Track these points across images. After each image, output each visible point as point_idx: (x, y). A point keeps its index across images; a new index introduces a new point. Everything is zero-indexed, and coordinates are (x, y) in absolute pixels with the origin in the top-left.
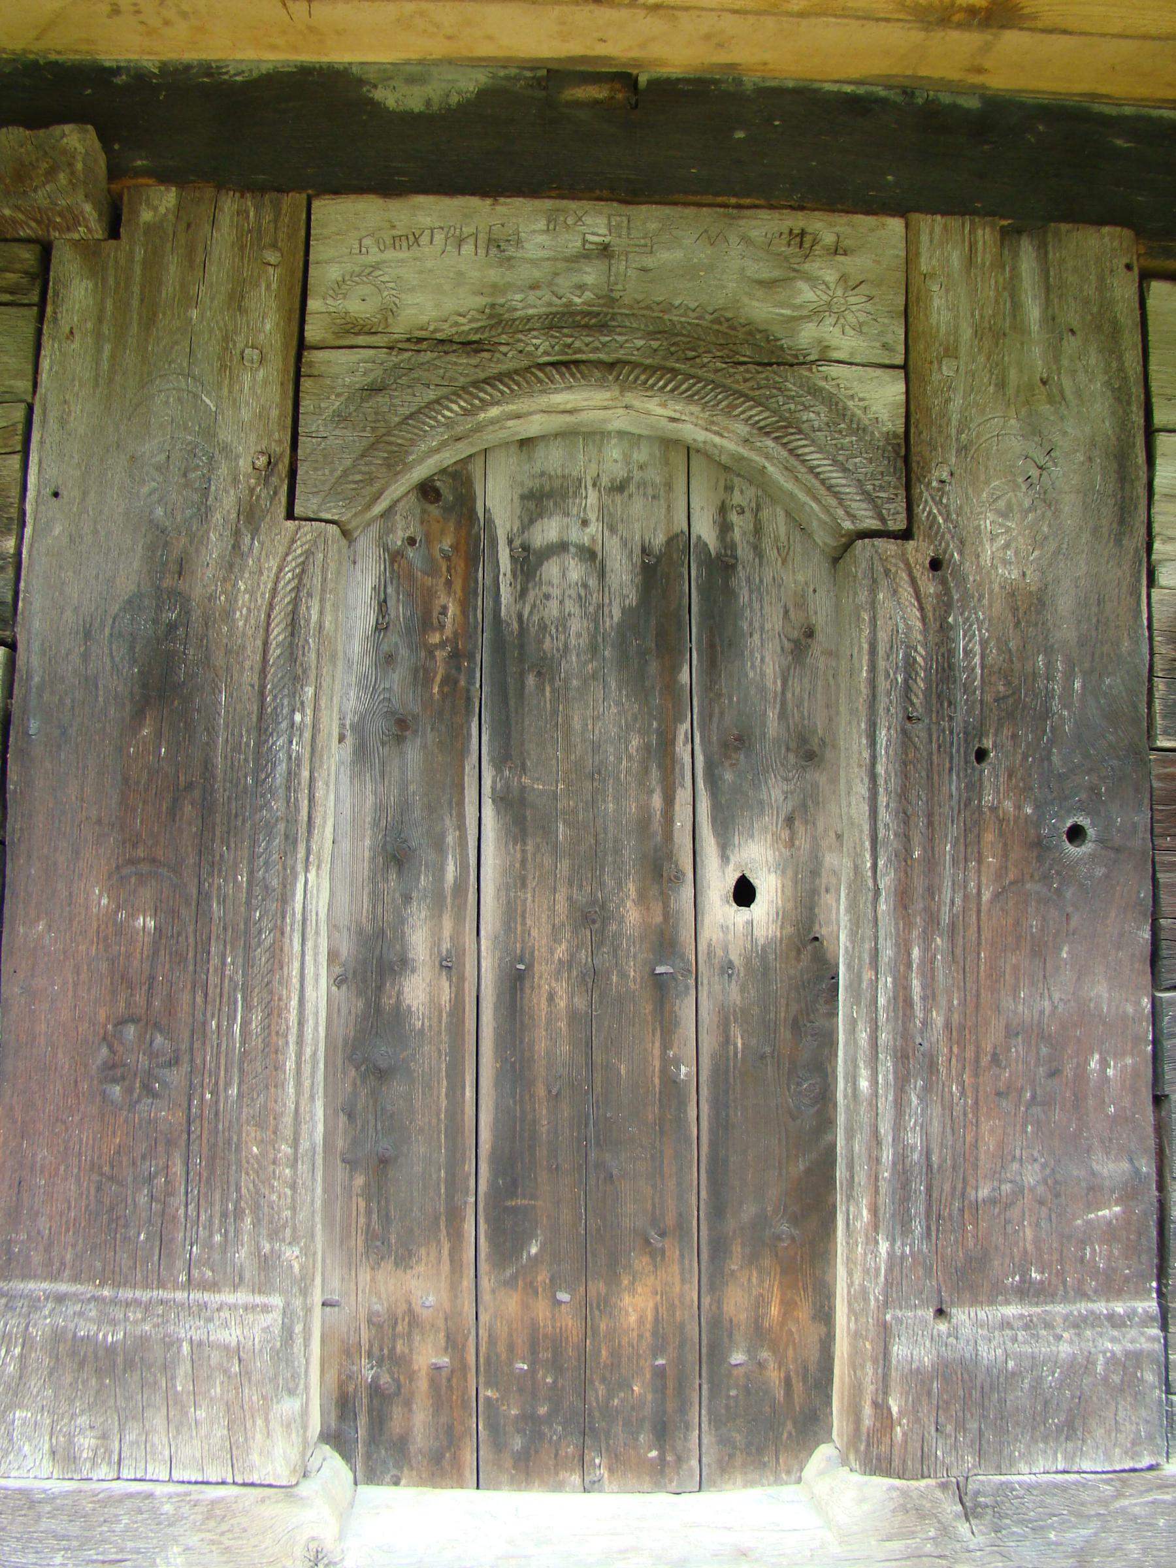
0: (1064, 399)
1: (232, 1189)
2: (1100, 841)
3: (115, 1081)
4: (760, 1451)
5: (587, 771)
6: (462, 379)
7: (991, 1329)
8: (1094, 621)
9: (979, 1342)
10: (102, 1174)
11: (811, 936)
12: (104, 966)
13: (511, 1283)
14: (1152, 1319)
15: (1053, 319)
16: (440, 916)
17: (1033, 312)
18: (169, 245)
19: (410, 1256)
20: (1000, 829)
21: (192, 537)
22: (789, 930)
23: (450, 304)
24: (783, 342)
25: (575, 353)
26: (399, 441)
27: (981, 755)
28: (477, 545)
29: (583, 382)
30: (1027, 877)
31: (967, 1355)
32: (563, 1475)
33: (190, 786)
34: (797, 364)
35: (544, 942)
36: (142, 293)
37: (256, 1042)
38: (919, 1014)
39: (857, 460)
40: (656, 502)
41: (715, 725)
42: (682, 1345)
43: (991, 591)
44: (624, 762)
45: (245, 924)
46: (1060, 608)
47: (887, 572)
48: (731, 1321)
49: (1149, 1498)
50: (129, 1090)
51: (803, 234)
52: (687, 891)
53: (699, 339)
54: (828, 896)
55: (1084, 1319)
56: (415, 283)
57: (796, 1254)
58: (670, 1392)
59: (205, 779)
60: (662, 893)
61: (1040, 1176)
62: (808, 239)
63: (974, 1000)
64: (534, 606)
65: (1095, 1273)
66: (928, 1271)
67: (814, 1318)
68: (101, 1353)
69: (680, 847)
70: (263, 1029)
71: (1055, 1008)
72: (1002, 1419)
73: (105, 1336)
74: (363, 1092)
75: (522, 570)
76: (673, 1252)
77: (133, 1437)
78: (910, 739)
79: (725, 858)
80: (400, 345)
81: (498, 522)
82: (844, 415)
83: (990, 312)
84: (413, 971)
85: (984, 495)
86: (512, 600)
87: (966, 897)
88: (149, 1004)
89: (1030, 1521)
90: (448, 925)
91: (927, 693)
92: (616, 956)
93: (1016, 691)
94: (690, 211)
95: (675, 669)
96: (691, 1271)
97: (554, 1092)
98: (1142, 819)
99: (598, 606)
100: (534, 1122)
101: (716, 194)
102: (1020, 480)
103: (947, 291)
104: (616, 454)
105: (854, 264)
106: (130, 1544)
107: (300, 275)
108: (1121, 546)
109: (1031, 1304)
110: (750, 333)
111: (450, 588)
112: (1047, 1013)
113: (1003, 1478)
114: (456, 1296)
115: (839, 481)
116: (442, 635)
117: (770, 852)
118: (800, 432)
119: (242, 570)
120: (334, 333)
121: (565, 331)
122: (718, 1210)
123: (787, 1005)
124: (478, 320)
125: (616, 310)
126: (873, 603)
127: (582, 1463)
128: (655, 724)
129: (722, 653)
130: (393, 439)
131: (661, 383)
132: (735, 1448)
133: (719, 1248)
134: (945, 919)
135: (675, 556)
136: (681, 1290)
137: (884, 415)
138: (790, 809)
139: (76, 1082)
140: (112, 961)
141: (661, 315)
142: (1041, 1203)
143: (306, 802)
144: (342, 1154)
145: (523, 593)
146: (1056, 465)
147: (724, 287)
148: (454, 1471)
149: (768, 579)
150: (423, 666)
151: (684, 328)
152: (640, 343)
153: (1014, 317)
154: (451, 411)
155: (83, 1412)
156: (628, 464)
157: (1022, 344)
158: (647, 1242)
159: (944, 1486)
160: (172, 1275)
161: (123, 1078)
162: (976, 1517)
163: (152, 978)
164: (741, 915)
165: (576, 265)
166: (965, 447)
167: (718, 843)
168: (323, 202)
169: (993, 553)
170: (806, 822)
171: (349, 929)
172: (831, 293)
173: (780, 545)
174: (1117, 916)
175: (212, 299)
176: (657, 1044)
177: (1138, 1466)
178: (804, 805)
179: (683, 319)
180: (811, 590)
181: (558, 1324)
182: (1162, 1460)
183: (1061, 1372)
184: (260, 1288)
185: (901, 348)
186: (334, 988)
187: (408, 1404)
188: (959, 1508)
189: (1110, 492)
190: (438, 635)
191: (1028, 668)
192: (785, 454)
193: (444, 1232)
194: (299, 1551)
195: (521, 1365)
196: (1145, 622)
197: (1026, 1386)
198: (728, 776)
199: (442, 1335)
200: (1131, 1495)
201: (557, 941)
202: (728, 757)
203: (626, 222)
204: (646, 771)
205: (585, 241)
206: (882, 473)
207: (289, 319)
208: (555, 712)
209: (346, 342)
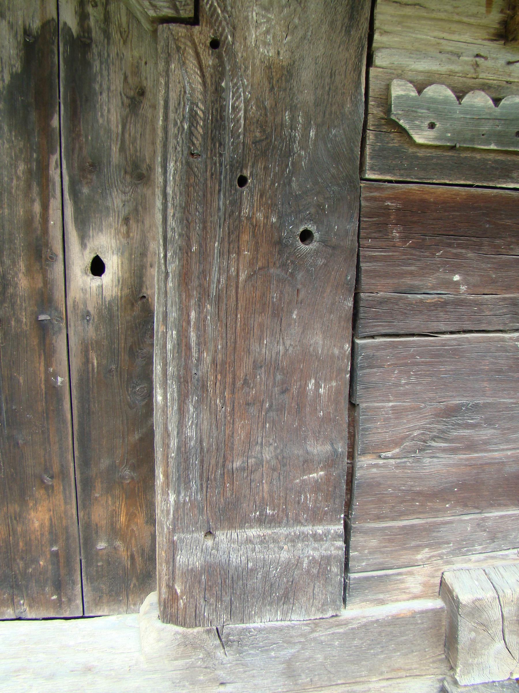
2: (323, 242)
4: (118, 594)
8: (327, 88)
9: (231, 552)
11: (141, 295)
14: (339, 536)
20: (254, 232)
22: (126, 291)
27: (242, 181)
30: (271, 265)
38: (195, 355)
41: (76, 156)
42: (67, 539)
43: (254, 65)
44: (15, 181)
46: (303, 79)
47: (178, 48)
48: (97, 525)
49: (331, 631)
52: (59, 267)
54: (152, 270)
55: (298, 537)
57: (135, 487)
58: (62, 564)
60: (41, 268)
61: (273, 454)
63: (233, 345)
65: (306, 509)
66: (201, 511)
67: (147, 522)
72: (244, 594)
76: (59, 487)
78: (191, 169)
79: (83, 245)
87: (228, 278)
89: (260, 647)
91: (204, 137)
92: (13, 309)
93: (268, 137)
95: (48, 117)
98: (352, 227)
108: (349, 35)
109: (265, 527)
112: (281, 354)
117: (113, 241)
123: (126, 339)
126: (167, 72)
128: (35, 155)
132: (102, 593)
134: (213, 292)
136: (65, 509)
138: (127, 212)
142: (274, 470)
149: (113, 55)
158: (43, 482)
159: (209, 632)
164: (94, 282)
167: (79, 235)
170: (138, 221)
173: (122, 30)
174: (331, 291)
176: (42, 364)
178: (136, 210)
180: (143, 63)
188: (218, 642)
191: (278, 120)
196: (363, 91)
197: (260, 576)
198: (85, 190)
202: (84, 177)
204: (29, 187)
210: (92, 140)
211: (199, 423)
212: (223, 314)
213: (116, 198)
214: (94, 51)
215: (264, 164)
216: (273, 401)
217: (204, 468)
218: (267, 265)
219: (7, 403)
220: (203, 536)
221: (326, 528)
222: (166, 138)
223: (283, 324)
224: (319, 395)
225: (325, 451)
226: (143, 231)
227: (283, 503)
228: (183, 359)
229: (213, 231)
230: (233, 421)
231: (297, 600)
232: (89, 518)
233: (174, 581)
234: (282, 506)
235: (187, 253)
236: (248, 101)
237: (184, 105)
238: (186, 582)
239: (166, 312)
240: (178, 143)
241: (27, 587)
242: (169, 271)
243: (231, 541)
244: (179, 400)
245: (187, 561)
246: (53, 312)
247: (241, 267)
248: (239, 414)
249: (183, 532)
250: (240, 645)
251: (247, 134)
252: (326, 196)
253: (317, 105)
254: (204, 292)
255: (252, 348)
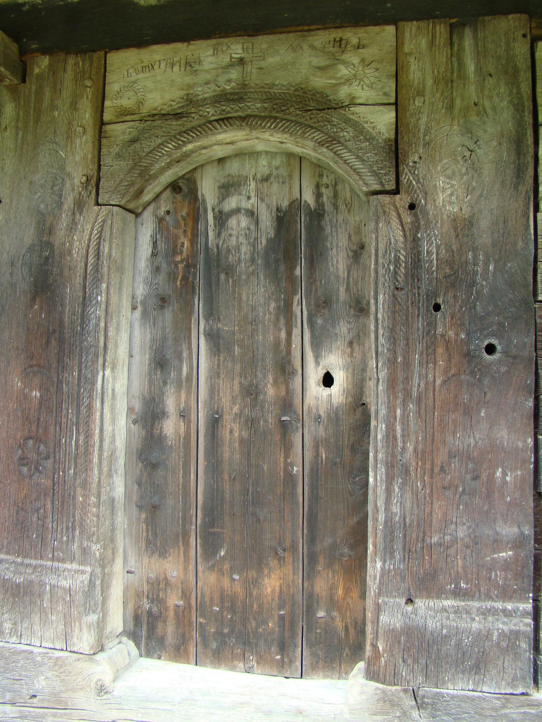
0: (485, 112)
1: (71, 516)
2: (505, 352)
3: (24, 465)
4: (332, 661)
5: (249, 320)
6: (173, 132)
7: (436, 612)
8: (502, 232)
9: (428, 618)
10: (19, 507)
11: (362, 402)
12: (19, 414)
13: (211, 568)
14: (528, 614)
15: (481, 69)
16: (180, 391)
17: (471, 67)
18: (46, 83)
19: (166, 553)
20: (447, 347)
21: (54, 216)
22: (350, 399)
23: (168, 96)
24: (331, 97)
25: (227, 113)
26: (145, 165)
27: (437, 308)
28: (198, 213)
29: (232, 128)
30: (462, 372)
31: (420, 624)
32: (236, 662)
33: (54, 331)
34: (340, 108)
35: (228, 404)
36: (35, 106)
37: (81, 450)
38: (400, 444)
39: (369, 155)
40: (284, 185)
41: (313, 295)
42: (293, 605)
43: (442, 219)
44: (267, 315)
45: (77, 394)
47: (385, 212)
48: (318, 595)
49: (522, 710)
50: (30, 470)
51: (341, 40)
52: (298, 379)
53: (288, 100)
54: (370, 382)
56: (152, 87)
57: (352, 564)
59: (61, 328)
60: (285, 380)
61: (466, 533)
62: (344, 43)
63: (431, 438)
64: (224, 240)
65: (497, 586)
66: (403, 579)
68: (14, 587)
69: (294, 358)
70: (85, 443)
71: (477, 443)
73: (16, 579)
74: (145, 474)
75: (219, 223)
77: (26, 625)
78: (397, 299)
79: (317, 363)
80: (145, 119)
81: (208, 200)
82: (362, 132)
83: (443, 69)
84: (168, 417)
85: (439, 168)
86: (214, 238)
87: (427, 383)
88: (37, 431)
89: (452, 714)
90: (183, 396)
91: (406, 275)
92: (262, 411)
94: (283, 36)
95: (293, 268)
96: (298, 569)
97: (232, 478)
99: (255, 238)
100: (223, 492)
101: (298, 26)
102: (459, 158)
103: (419, 61)
104: (265, 163)
105: (368, 53)
106: (23, 673)
107: (101, 90)
108: (518, 190)
109: (460, 600)
110: (314, 95)
111: (186, 233)
112: (472, 445)
113: (438, 690)
114: (186, 573)
115: (359, 166)
116: (182, 256)
117: (340, 360)
118: (339, 142)
119: (75, 231)
120: (116, 116)
121: (222, 103)
122: (312, 540)
123: (349, 438)
124: (181, 102)
125: (247, 90)
126: (377, 229)
127: (244, 658)
129: (317, 259)
130: (142, 164)
131: (269, 124)
133: (312, 559)
134: (415, 394)
135: (293, 211)
136: (293, 578)
137: (384, 129)
139: (8, 465)
140: (23, 411)
141: (269, 90)
142: (467, 547)
143: (103, 338)
144: (136, 503)
145: (219, 234)
146: (480, 149)
147: (300, 73)
148: (185, 655)
149: (340, 220)
150: (173, 272)
151: (281, 95)
152: (259, 105)
153: (460, 71)
154: (169, 148)
155: (6, 613)
156: (270, 167)
157: (464, 85)
158: (276, 553)
159: (405, 691)
160: (46, 554)
161: (27, 464)
162: (422, 709)
163: (39, 419)
164: (326, 392)
165: (227, 70)
166: (428, 143)
167: (314, 355)
168: (112, 54)
169: (443, 198)
170: (359, 344)
171: (139, 398)
172: (356, 69)
173: (347, 202)
174: (513, 394)
175: (64, 106)
176: (282, 456)
177: (515, 692)
178: (358, 335)
179: (280, 91)
181: (234, 590)
182: (531, 691)
183: (472, 638)
184: (82, 563)
185: (393, 94)
186: (132, 425)
187: (165, 622)
188: (414, 703)
189: (512, 161)
190: (180, 257)
191: (463, 259)
192: (332, 155)
193: (181, 542)
194: (93, 685)
195: (216, 608)
198: (320, 321)
199: (180, 591)
200: (511, 708)
201: (234, 403)
203: (251, 46)
204: (278, 320)
205: (231, 58)
206: (382, 161)
207: (96, 112)
208: (234, 291)
209: (121, 120)
210: (325, 283)
211: (403, 502)
212: (422, 412)
213: (342, 326)
214: (327, 219)
215: (453, 293)
216: (466, 486)
217: (407, 541)
218: (458, 372)
219: (253, 486)
220: (404, 602)
221: (516, 605)
222: (377, 277)
223: (473, 421)
224: (506, 482)
225: (512, 533)
226: (363, 352)
227: (475, 578)
228: (390, 448)
229: (414, 346)
230: (432, 502)
231: (488, 671)
232: (312, 588)
233: (377, 640)
234: (475, 581)
235: (394, 364)
236: (439, 246)
237: (390, 253)
238: (387, 641)
239: (378, 410)
240: (385, 280)
241: (256, 645)
242: (380, 377)
243: (429, 608)
244: (386, 481)
245: (388, 622)
246: (292, 415)
247: (437, 374)
248: (436, 496)
249: (387, 597)
250: (434, 709)
251: (439, 271)
252: (506, 316)
253: (494, 246)
254: (407, 394)
255: (447, 440)
